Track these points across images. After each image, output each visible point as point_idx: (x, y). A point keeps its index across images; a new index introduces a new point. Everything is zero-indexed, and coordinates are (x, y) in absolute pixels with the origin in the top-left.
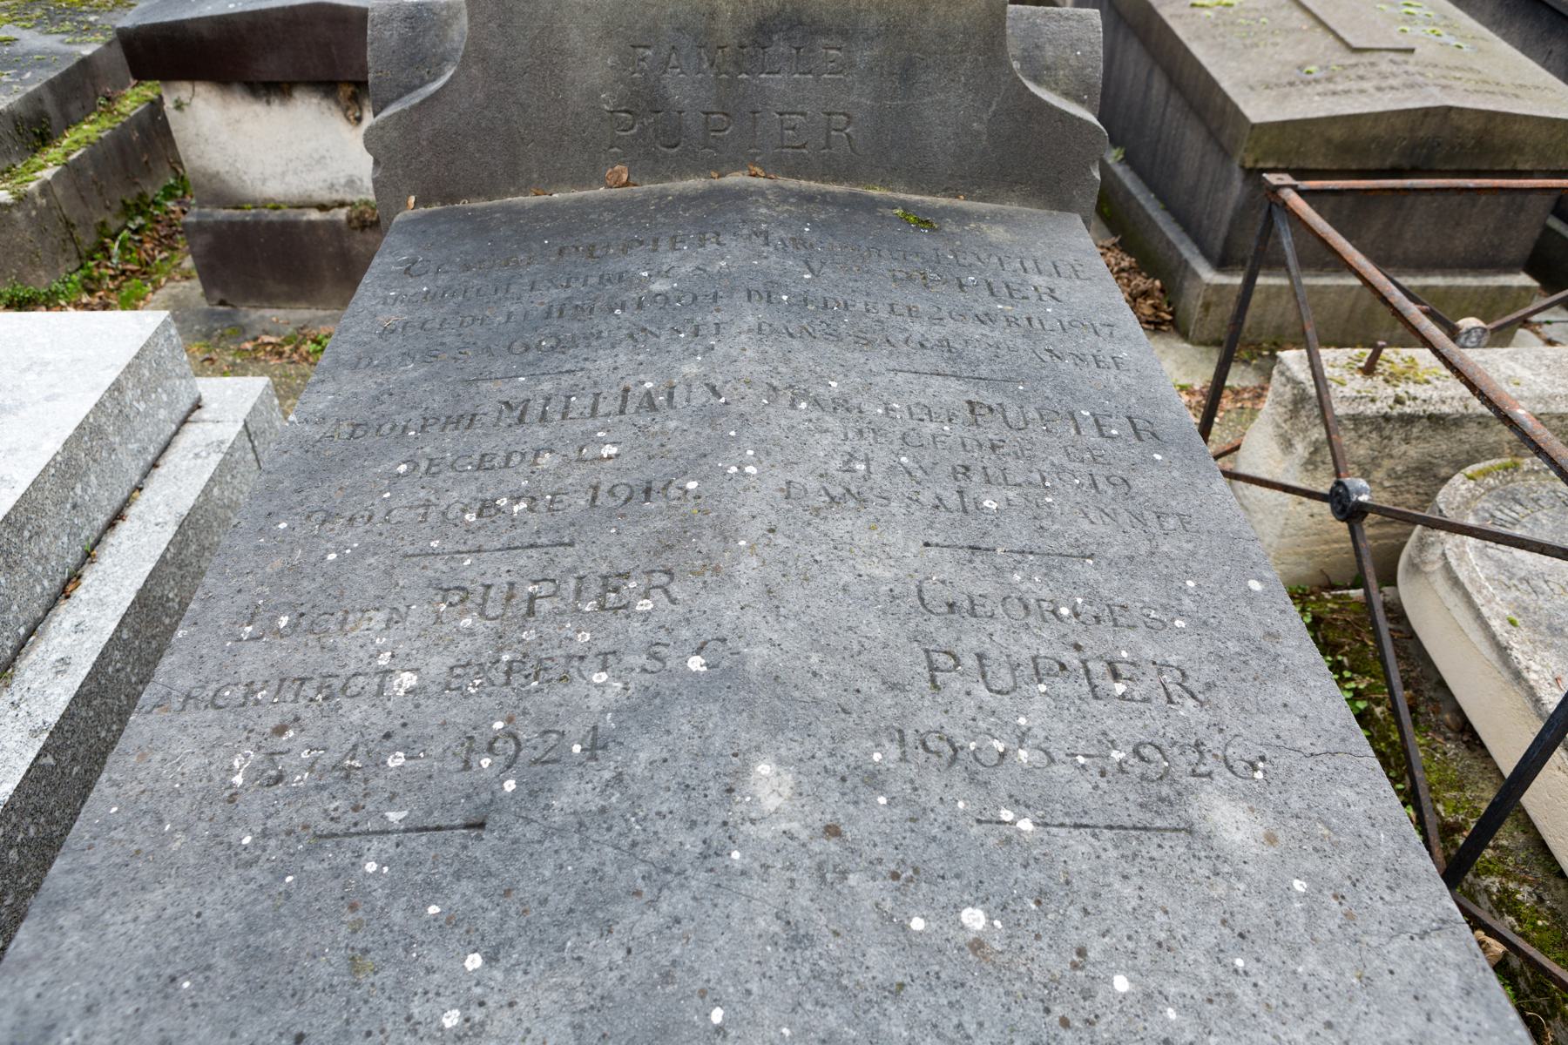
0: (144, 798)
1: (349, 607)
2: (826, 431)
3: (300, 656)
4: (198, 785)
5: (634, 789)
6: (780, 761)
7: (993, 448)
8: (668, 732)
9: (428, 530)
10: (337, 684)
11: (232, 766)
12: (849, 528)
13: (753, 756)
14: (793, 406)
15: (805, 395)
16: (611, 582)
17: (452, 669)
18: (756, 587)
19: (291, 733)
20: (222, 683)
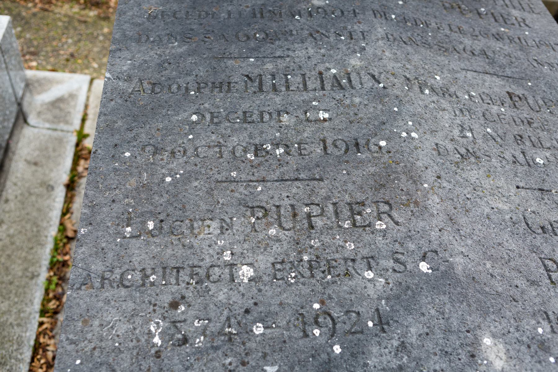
0: (96, 353)
1: (192, 217)
2: (444, 110)
3: (172, 254)
4: (131, 345)
5: (415, 353)
6: (494, 336)
7: (529, 123)
8: (423, 314)
9: (225, 164)
10: (202, 272)
11: (150, 330)
12: (477, 176)
13: (478, 332)
14: (422, 92)
15: (426, 85)
16: (356, 207)
17: (273, 264)
18: (442, 217)
19: (182, 308)
20: (124, 269)
